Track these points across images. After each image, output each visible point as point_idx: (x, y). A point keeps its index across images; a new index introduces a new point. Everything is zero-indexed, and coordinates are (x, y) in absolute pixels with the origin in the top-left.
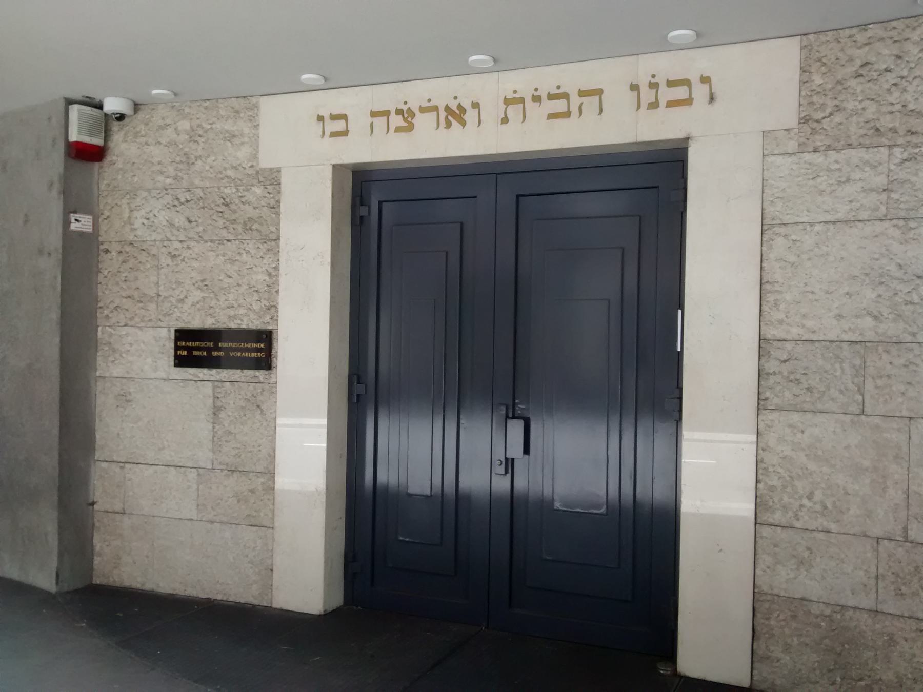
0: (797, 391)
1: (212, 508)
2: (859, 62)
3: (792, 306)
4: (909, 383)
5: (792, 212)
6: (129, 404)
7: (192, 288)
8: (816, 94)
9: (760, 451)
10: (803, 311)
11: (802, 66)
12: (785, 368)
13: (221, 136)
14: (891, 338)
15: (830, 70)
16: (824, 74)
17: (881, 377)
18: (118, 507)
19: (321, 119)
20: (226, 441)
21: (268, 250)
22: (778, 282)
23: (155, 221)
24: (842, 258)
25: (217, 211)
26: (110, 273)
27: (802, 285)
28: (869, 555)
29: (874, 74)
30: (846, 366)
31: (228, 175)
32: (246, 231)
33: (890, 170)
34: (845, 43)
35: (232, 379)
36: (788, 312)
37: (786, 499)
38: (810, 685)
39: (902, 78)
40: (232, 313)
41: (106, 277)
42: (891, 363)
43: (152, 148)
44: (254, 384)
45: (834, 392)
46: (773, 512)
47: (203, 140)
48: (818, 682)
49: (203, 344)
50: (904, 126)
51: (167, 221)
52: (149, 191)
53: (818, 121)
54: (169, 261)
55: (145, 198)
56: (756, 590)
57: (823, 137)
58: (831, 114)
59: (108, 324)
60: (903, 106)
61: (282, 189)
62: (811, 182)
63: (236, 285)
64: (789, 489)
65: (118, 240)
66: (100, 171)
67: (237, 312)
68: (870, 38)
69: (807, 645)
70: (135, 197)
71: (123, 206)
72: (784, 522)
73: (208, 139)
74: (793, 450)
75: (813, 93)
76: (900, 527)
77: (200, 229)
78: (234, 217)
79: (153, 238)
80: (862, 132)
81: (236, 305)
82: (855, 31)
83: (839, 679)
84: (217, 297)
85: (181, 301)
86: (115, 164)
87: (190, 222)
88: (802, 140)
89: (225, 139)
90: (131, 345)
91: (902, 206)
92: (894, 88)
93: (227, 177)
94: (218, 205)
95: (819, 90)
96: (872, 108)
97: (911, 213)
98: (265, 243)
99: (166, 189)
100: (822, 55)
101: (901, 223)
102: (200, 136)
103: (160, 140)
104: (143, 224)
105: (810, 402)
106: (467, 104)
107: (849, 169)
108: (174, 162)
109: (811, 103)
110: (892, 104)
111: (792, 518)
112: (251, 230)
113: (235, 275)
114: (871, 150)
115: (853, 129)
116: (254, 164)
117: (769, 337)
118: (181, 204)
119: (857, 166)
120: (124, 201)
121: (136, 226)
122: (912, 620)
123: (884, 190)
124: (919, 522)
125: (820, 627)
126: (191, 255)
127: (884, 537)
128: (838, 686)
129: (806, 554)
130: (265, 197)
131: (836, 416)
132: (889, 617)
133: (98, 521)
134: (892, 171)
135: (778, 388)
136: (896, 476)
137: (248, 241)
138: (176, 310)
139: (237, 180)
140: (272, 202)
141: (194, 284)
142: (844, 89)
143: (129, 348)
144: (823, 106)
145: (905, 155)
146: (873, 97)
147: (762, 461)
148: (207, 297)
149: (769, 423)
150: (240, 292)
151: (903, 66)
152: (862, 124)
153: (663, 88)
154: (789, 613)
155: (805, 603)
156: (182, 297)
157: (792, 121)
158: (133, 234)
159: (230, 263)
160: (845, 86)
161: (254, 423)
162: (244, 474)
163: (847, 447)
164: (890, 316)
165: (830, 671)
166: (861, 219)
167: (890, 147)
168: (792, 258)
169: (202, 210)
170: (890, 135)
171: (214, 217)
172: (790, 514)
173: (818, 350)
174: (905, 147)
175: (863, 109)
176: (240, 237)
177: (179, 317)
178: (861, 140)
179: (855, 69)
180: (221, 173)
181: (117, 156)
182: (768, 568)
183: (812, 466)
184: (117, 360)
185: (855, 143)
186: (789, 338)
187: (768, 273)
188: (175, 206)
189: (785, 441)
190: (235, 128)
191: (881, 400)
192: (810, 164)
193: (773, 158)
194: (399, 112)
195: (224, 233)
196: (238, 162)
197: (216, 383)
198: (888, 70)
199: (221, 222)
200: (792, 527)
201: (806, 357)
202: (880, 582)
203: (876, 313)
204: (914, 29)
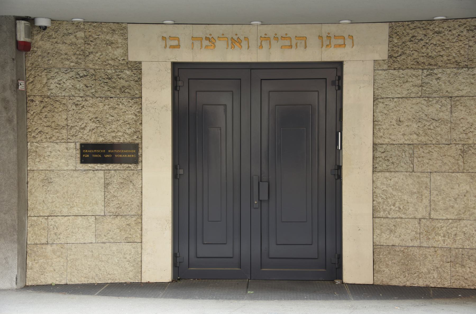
0: (388, 164)
1: (105, 235)
2: (411, 35)
3: (385, 130)
4: (430, 159)
5: (385, 93)
6: (51, 184)
7: (90, 122)
8: (395, 47)
9: (374, 189)
10: (390, 132)
11: (390, 34)
12: (383, 155)
13: (104, 43)
14: (423, 142)
15: (400, 37)
16: (398, 39)
17: (420, 157)
18: (44, 241)
19: (164, 38)
20: (112, 201)
21: (135, 103)
22: (380, 121)
23: (64, 85)
24: (405, 112)
25: (104, 82)
26: (35, 113)
27: (389, 122)
28: (417, 225)
29: (417, 41)
30: (407, 154)
31: (110, 63)
32: (121, 93)
33: (422, 78)
34: (406, 27)
36: (384, 133)
37: (385, 207)
38: (396, 279)
39: (427, 43)
40: (113, 134)
41: (32, 115)
42: (423, 152)
43: (60, 45)
44: (128, 171)
45: (402, 164)
46: (380, 212)
47: (93, 44)
48: (399, 277)
49: (98, 151)
50: (427, 62)
51: (73, 86)
52: (60, 69)
53: (396, 58)
54: (74, 107)
55: (57, 72)
56: (374, 244)
57: (397, 64)
58: (400, 55)
59: (35, 141)
60: (427, 54)
61: (142, 72)
62: (393, 82)
63: (116, 120)
64: (386, 203)
65: (39, 95)
66: (26, 55)
67: (117, 134)
68: (415, 26)
69: (395, 263)
70: (50, 71)
71: (43, 76)
72: (384, 216)
73: (97, 43)
74: (387, 187)
75: (393, 46)
76: (428, 214)
77: (93, 91)
78: (114, 85)
79: (63, 95)
80: (412, 63)
81: (116, 131)
82: (410, 23)
83: (407, 275)
84: (105, 127)
85: (83, 128)
86: (36, 52)
87: (87, 87)
88: (389, 65)
89: (107, 44)
91: (427, 92)
92: (424, 47)
93: (109, 64)
94: (104, 79)
95: (396, 45)
96: (416, 54)
97: (430, 95)
98: (133, 99)
99: (71, 69)
100: (397, 31)
101: (427, 99)
102: (91, 41)
103: (65, 41)
104: (57, 86)
105: (393, 168)
106: (242, 38)
107: (407, 77)
108: (76, 54)
109: (393, 50)
110: (423, 53)
111: (387, 214)
112: (125, 92)
113: (116, 115)
114: (415, 70)
115: (409, 61)
117: (377, 143)
118: (81, 77)
119: (410, 76)
122: (433, 248)
123: (420, 86)
124: (434, 211)
125: (399, 255)
126: (88, 104)
127: (422, 218)
128: (407, 277)
129: (393, 228)
130: (132, 76)
131: (403, 173)
132: (425, 248)
134: (423, 79)
135: (381, 163)
136: (426, 195)
137: (123, 98)
138: (79, 133)
139: (115, 66)
140: (136, 79)
141: (90, 120)
142: (406, 45)
143: (49, 154)
146: (417, 50)
147: (375, 192)
148: (99, 127)
149: (377, 177)
150: (118, 124)
151: (427, 39)
152: (412, 60)
153: (333, 39)
154: (387, 252)
155: (393, 247)
156: (83, 126)
157: (386, 57)
158: (50, 92)
159: (112, 109)
160: (406, 44)
161: (129, 190)
162: (123, 217)
163: (408, 185)
164: (423, 134)
165: (404, 272)
166: (412, 97)
167: (423, 70)
168: (386, 112)
169: (94, 81)
170: (422, 65)
172: (387, 212)
173: (396, 148)
174: (427, 69)
175: (413, 54)
176: (118, 96)
177: (81, 137)
178: (412, 66)
179: (409, 38)
181: (37, 48)
182: (379, 235)
183: (394, 193)
184: (42, 161)
185: (410, 67)
186: (385, 143)
187: (376, 117)
188: (77, 78)
189: (384, 184)
190: (113, 39)
191: (420, 166)
192: (392, 74)
193: (378, 71)
194: (207, 39)
195: (108, 93)
196: (116, 57)
197: (106, 171)
198: (421, 40)
199: (106, 88)
200: (387, 218)
201: (391, 150)
202: (421, 235)
203: (417, 133)
204: (431, 25)
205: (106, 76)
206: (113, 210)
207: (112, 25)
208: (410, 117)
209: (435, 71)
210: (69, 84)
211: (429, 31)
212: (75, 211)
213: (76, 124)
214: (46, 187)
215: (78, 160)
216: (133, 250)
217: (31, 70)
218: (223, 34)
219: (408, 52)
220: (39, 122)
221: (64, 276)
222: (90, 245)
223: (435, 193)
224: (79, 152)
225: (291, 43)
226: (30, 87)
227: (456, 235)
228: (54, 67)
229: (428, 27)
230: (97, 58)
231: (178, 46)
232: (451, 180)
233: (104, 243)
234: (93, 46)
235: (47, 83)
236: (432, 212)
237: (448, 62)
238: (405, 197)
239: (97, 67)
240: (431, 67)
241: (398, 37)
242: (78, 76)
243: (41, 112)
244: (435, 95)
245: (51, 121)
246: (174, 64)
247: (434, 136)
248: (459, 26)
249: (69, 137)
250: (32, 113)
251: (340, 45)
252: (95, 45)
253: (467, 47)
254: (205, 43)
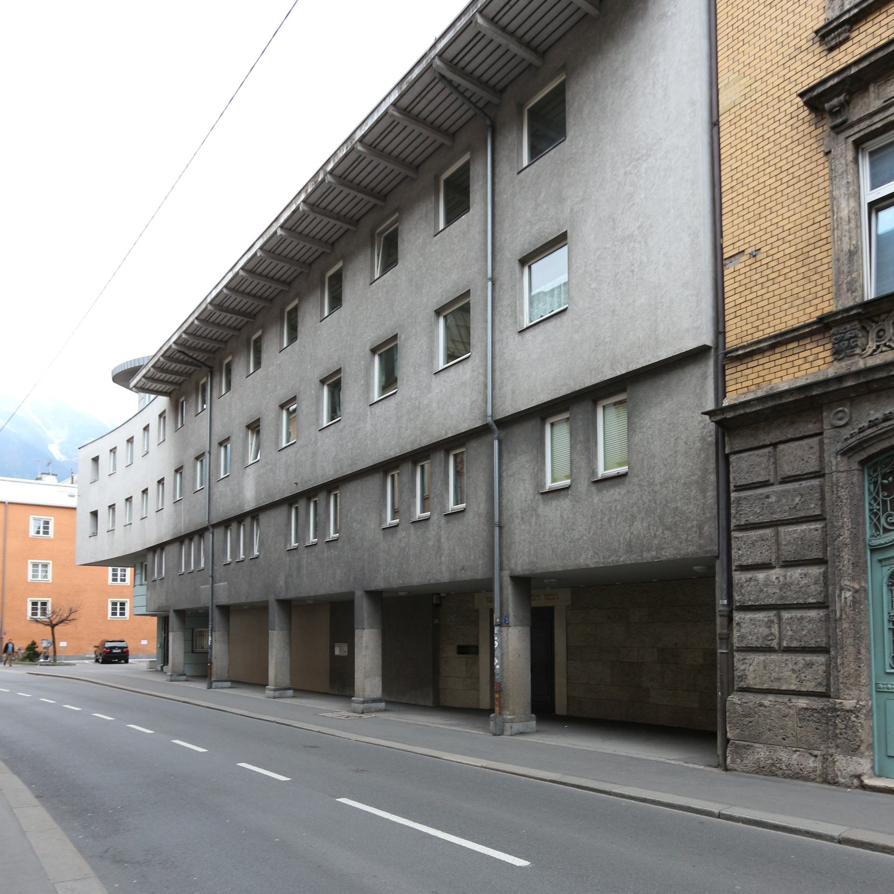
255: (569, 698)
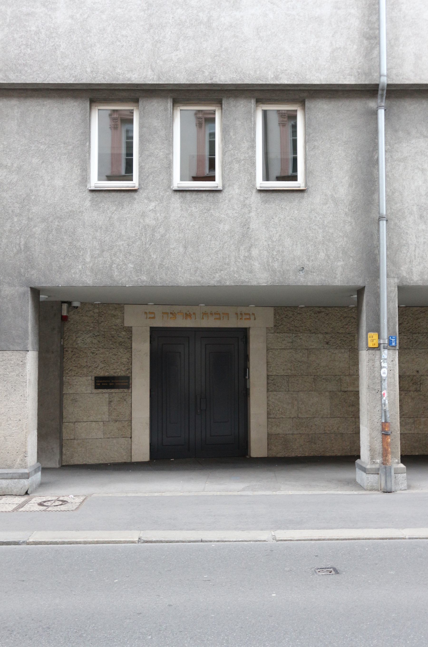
2: (286, 315)
7: (100, 363)
12: (272, 382)
18: (72, 437)
19: (146, 313)
35: (116, 392)
37: (274, 412)
40: (115, 371)
43: (84, 317)
46: (271, 415)
47: (104, 316)
49: (106, 381)
52: (84, 331)
53: (278, 326)
54: (91, 354)
67: (117, 371)
77: (103, 344)
81: (116, 369)
82: (284, 308)
85: (96, 367)
90: (77, 382)
96: (289, 325)
99: (90, 331)
101: (295, 350)
102: (103, 315)
106: (192, 313)
109: (276, 322)
116: (123, 325)
118: (96, 336)
120: (74, 334)
121: (78, 342)
133: (65, 443)
140: (129, 337)
141: (101, 362)
144: (279, 323)
145: (295, 335)
153: (243, 315)
156: (96, 366)
157: (272, 326)
161: (123, 405)
168: (273, 357)
171: (108, 341)
180: (110, 327)
183: (279, 403)
188: (93, 337)
190: (115, 313)
194: (171, 313)
195: (112, 346)
198: (291, 317)
199: (111, 343)
205: (111, 336)
206: (114, 418)
207: (115, 306)
208: (287, 360)
209: (299, 335)
210: (89, 340)
211: (295, 313)
212: (91, 419)
213: (92, 365)
214: (74, 404)
215: (93, 387)
216: (126, 442)
217: (67, 332)
218: (180, 311)
219: (284, 324)
220: (70, 364)
221: (84, 459)
222: (100, 439)
223: (301, 403)
224: (94, 382)
225: (220, 317)
226: (65, 343)
227: (311, 426)
228: (80, 330)
229: (294, 310)
230: (105, 325)
231: (154, 318)
232: (309, 396)
233: (109, 438)
234: (103, 318)
235: (75, 340)
236: (299, 414)
237: (305, 330)
238: (285, 406)
239: (106, 330)
240: (296, 332)
241: (279, 315)
242: (94, 336)
243: (72, 358)
244: (299, 348)
245: (78, 363)
246: (151, 328)
247: (299, 371)
248: (310, 311)
249: (88, 373)
250: (66, 358)
251: (248, 319)
252: (105, 317)
253: (314, 322)
254: (171, 316)
255: (270, 436)
